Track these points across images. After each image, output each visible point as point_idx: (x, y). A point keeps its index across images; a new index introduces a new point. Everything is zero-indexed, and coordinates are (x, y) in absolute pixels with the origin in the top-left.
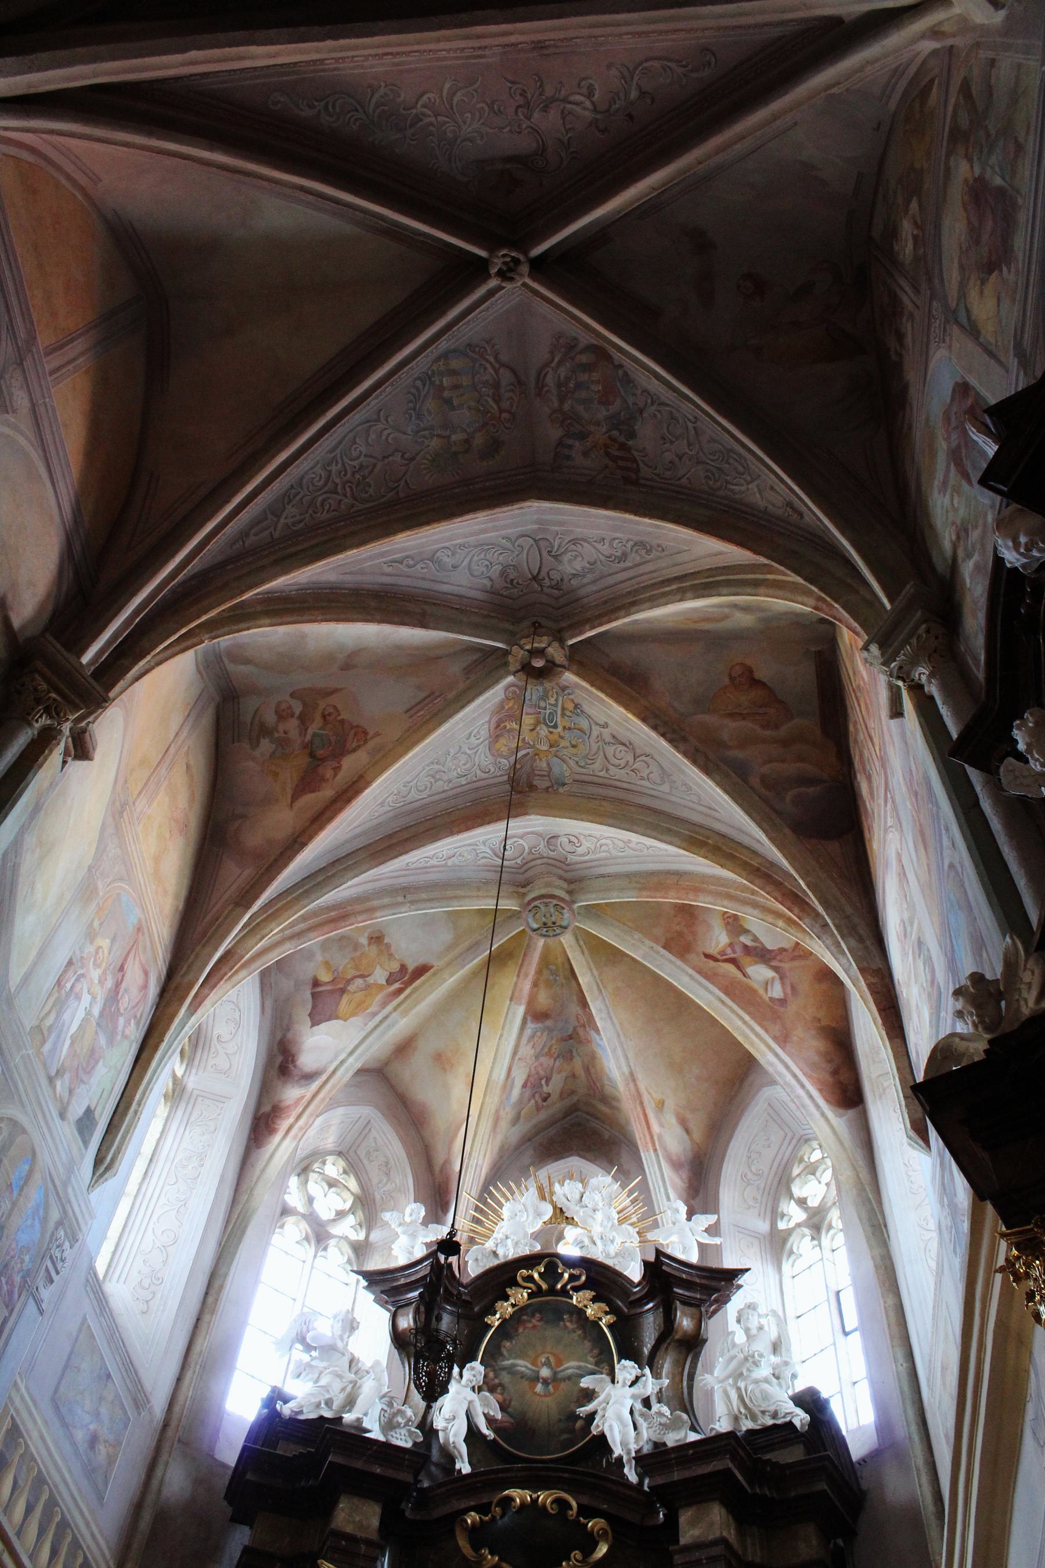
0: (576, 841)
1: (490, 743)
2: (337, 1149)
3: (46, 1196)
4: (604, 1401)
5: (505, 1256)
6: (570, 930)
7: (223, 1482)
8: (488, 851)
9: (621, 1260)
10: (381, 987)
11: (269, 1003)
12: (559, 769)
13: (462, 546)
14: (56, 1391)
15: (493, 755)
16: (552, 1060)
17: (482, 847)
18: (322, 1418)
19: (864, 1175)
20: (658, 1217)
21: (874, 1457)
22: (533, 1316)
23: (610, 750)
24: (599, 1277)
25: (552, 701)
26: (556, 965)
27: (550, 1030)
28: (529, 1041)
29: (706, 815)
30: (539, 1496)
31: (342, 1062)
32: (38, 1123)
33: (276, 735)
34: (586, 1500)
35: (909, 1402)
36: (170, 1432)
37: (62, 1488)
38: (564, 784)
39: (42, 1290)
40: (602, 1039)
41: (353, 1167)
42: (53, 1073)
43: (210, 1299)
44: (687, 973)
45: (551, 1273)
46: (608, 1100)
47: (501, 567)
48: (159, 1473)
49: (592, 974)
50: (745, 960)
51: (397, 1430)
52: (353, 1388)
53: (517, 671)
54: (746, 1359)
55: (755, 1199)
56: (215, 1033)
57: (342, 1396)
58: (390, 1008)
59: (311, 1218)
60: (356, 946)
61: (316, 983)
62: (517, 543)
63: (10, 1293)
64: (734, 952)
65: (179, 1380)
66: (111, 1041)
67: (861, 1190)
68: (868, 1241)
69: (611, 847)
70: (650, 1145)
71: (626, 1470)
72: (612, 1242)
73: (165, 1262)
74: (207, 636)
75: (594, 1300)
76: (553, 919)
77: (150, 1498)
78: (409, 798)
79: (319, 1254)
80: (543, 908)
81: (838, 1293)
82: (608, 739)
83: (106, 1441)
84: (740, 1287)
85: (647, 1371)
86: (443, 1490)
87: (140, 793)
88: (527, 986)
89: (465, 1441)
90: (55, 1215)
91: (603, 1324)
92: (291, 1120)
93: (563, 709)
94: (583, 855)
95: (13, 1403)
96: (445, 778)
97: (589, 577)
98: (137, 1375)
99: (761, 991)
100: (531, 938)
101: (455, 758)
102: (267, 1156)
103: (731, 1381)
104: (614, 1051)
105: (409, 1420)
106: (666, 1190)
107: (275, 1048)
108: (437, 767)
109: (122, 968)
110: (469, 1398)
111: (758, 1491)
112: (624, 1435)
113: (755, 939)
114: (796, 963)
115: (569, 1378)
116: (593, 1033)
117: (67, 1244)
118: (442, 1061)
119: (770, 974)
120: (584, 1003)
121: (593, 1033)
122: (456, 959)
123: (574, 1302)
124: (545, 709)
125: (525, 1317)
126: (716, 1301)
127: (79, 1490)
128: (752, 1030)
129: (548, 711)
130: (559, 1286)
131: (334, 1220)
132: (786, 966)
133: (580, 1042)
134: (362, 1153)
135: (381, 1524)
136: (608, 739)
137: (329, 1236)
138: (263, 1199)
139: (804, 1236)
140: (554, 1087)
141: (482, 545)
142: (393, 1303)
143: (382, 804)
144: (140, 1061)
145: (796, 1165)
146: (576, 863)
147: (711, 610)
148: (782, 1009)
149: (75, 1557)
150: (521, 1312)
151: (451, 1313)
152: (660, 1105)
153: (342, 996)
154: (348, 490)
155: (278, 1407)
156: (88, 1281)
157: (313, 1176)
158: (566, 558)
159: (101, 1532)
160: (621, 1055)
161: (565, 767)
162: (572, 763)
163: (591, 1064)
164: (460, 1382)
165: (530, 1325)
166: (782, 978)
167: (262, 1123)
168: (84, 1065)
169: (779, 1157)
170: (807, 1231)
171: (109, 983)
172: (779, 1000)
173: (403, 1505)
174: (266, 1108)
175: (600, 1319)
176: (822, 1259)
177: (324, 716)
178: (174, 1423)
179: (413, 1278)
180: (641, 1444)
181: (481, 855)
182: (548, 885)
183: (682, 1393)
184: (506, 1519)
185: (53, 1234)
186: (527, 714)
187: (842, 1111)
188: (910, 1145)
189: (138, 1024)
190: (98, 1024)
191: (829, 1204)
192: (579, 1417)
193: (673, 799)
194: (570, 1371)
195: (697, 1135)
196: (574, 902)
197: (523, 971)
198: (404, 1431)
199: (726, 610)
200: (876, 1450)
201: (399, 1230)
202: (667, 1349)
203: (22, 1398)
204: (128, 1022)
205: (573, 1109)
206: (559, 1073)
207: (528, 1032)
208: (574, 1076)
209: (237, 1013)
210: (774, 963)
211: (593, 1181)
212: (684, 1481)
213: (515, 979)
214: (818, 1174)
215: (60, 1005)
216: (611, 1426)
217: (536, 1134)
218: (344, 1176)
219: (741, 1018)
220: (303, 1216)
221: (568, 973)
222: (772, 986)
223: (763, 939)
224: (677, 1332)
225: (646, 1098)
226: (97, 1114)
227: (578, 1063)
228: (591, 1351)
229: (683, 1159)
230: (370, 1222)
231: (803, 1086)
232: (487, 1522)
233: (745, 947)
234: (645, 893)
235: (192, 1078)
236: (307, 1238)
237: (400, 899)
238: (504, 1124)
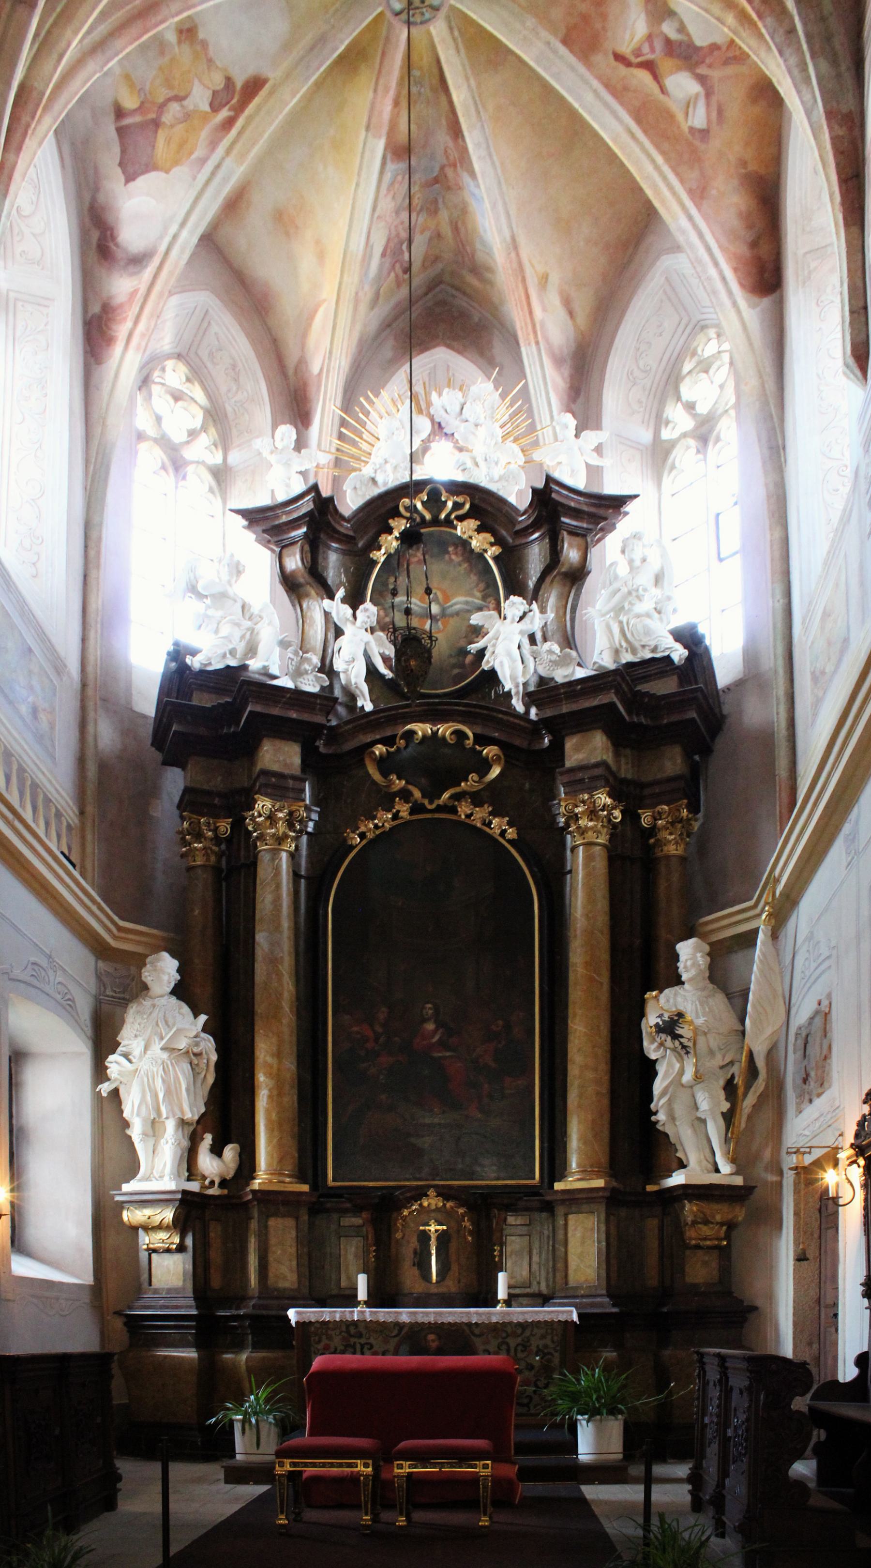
2: (177, 350)
4: (493, 638)
5: (385, 484)
7: (146, 733)
9: (505, 484)
10: (205, 118)
11: (66, 149)
18: (228, 667)
19: (771, 385)
20: (540, 433)
21: (739, 685)
24: (483, 505)
26: (421, 69)
28: (389, 190)
30: (438, 729)
31: (175, 237)
34: (479, 730)
35: (779, 637)
36: (90, 692)
37: (26, 758)
40: (478, 186)
41: (197, 374)
44: (591, 87)
46: (480, 270)
48: (90, 728)
50: (665, 65)
51: (305, 676)
52: (252, 633)
54: (630, 593)
55: (640, 402)
59: (163, 442)
61: (119, 113)
64: (653, 50)
65: (84, 640)
67: (765, 403)
68: (764, 463)
70: (532, 337)
71: (514, 701)
72: (496, 463)
75: (479, 530)
77: (90, 752)
81: (718, 515)
83: (44, 710)
84: (626, 514)
85: (535, 606)
86: (350, 726)
89: (365, 681)
91: (488, 556)
92: (129, 324)
99: (680, 117)
100: (390, 26)
102: (112, 373)
103: (612, 614)
104: (494, 206)
106: (547, 393)
107: (87, 220)
110: (366, 640)
111: (635, 720)
112: (513, 669)
113: (682, 29)
115: (457, 614)
118: (285, 222)
120: (456, 131)
121: (466, 178)
123: (459, 532)
126: (602, 529)
127: (38, 757)
128: (665, 179)
130: (443, 516)
131: (188, 443)
132: (715, 74)
133: (449, 188)
134: (204, 354)
137: (186, 463)
138: (117, 429)
139: (688, 448)
142: (277, 543)
145: (688, 359)
149: (50, 810)
151: (336, 550)
152: (544, 280)
153: (156, 132)
157: (156, 389)
160: (505, 217)
163: (461, 222)
164: (354, 624)
166: (708, 95)
167: (96, 330)
169: (671, 348)
170: (692, 442)
173: (317, 744)
174: (96, 309)
175: (486, 551)
176: (705, 476)
178: (91, 684)
179: (295, 515)
180: (528, 677)
183: (566, 625)
184: (409, 749)
187: (756, 299)
188: (844, 373)
191: (720, 411)
192: (469, 652)
194: (458, 607)
195: (582, 318)
197: (382, 82)
198: (311, 677)
200: (740, 680)
201: (273, 459)
202: (552, 581)
205: (434, 284)
207: (388, 176)
210: (702, 70)
211: (474, 389)
212: (572, 714)
213: (371, 94)
214: (711, 372)
216: (501, 663)
217: (396, 318)
218: (188, 385)
220: (155, 440)
221: (435, 81)
222: (695, 108)
223: (691, 29)
224: (563, 565)
225: (529, 271)
227: (444, 215)
228: (477, 585)
229: (565, 351)
230: (224, 443)
231: (716, 264)
232: (393, 753)
233: (668, 42)
238: (363, 308)
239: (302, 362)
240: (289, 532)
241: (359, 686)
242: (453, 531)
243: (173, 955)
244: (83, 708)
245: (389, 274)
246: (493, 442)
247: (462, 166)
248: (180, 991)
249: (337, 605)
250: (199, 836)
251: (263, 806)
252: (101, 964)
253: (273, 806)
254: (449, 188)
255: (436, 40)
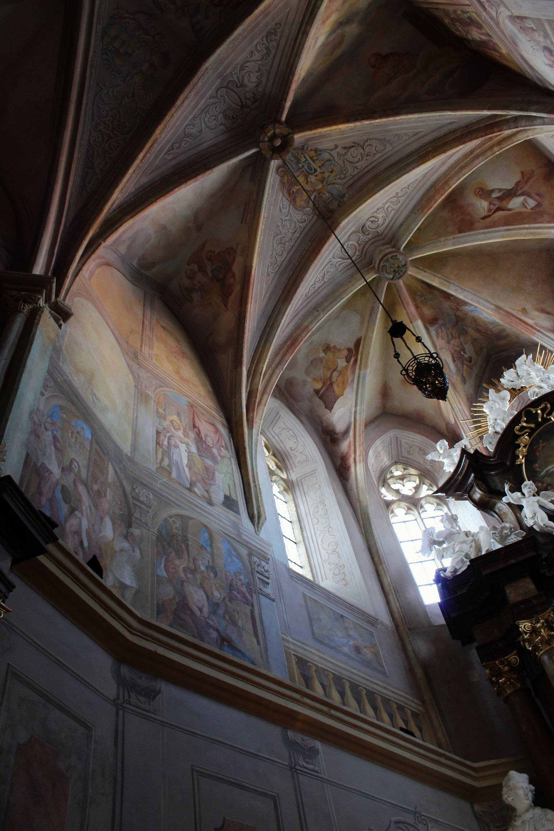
0: (374, 219)
1: (293, 206)
2: (393, 461)
3: (228, 541)
6: (408, 264)
7: (446, 633)
8: (339, 260)
11: (303, 419)
12: (337, 188)
13: (194, 118)
14: (313, 634)
15: (300, 211)
16: (457, 339)
17: (334, 260)
22: (539, 443)
23: (349, 157)
25: (303, 159)
26: (419, 291)
27: (444, 325)
28: (438, 337)
29: (417, 140)
31: (355, 412)
32: (199, 513)
33: (196, 287)
36: (401, 628)
38: (344, 195)
39: (265, 590)
41: (407, 463)
42: (188, 486)
43: (376, 559)
45: (531, 417)
47: (221, 115)
48: (409, 648)
49: (438, 277)
53: (272, 156)
56: (288, 448)
57: (472, 550)
58: (357, 371)
59: (404, 498)
60: (321, 361)
61: (317, 392)
62: (219, 96)
63: (245, 597)
64: (495, 205)
66: (214, 459)
69: (392, 205)
70: (534, 330)
73: (339, 557)
74: (101, 240)
76: (397, 265)
78: (279, 263)
79: (421, 511)
80: (387, 264)
82: (343, 152)
83: (365, 647)
87: (141, 346)
88: (412, 309)
89: (549, 520)
90: (244, 552)
92: (353, 456)
93: (311, 158)
94: (383, 223)
95: (290, 648)
96: (287, 239)
97: (264, 79)
98: (360, 610)
99: (524, 210)
100: (395, 284)
101: (283, 226)
102: (354, 479)
105: (511, 528)
108: (279, 237)
109: (194, 426)
113: (500, 190)
114: (530, 183)
116: (466, 308)
117: (263, 563)
119: (521, 199)
120: (448, 296)
121: (466, 308)
122: (368, 324)
124: (303, 166)
125: (535, 447)
127: (369, 675)
128: (534, 228)
129: (306, 167)
131: (416, 492)
132: (526, 188)
133: (463, 319)
134: (405, 454)
135: (535, 584)
136: (343, 152)
140: (470, 351)
141: (203, 111)
142: (465, 492)
143: (268, 275)
144: (242, 465)
146: (385, 230)
147: (332, 38)
148: (541, 208)
150: (531, 448)
151: (497, 475)
152: (524, 311)
153: (333, 387)
154: (116, 132)
155: (442, 575)
156: (291, 576)
157: (390, 481)
158: (246, 81)
159: (396, 688)
161: (337, 186)
162: (338, 181)
163: (479, 326)
165: (540, 449)
167: (341, 470)
168: (206, 476)
171: (192, 435)
172: (536, 206)
174: (339, 462)
177: (209, 260)
179: (464, 472)
181: (337, 265)
182: (381, 252)
185: (250, 562)
186: (298, 177)
189: (226, 449)
190: (200, 456)
193: (397, 149)
196: (399, 249)
199: (339, 31)
203: (294, 644)
204: (219, 450)
206: (466, 343)
207: (433, 333)
208: (475, 340)
209: (291, 432)
210: (520, 192)
215: (167, 453)
219: (524, 228)
220: (399, 500)
222: (527, 203)
225: (513, 312)
226: (233, 497)
227: (471, 331)
233: (498, 198)
234: (425, 210)
235: (293, 475)
236: (409, 509)
237: (316, 313)
239: (447, 424)
240: (467, 482)
241: (547, 524)
242: (551, 422)
243: (520, 771)
244: (401, 639)
245: (463, 367)
246: (541, 373)
247: (460, 306)
248: (541, 800)
249: (509, 495)
250: (499, 674)
251: (524, 627)
252: (477, 807)
253: (532, 623)
254: (463, 319)
255: (414, 274)
